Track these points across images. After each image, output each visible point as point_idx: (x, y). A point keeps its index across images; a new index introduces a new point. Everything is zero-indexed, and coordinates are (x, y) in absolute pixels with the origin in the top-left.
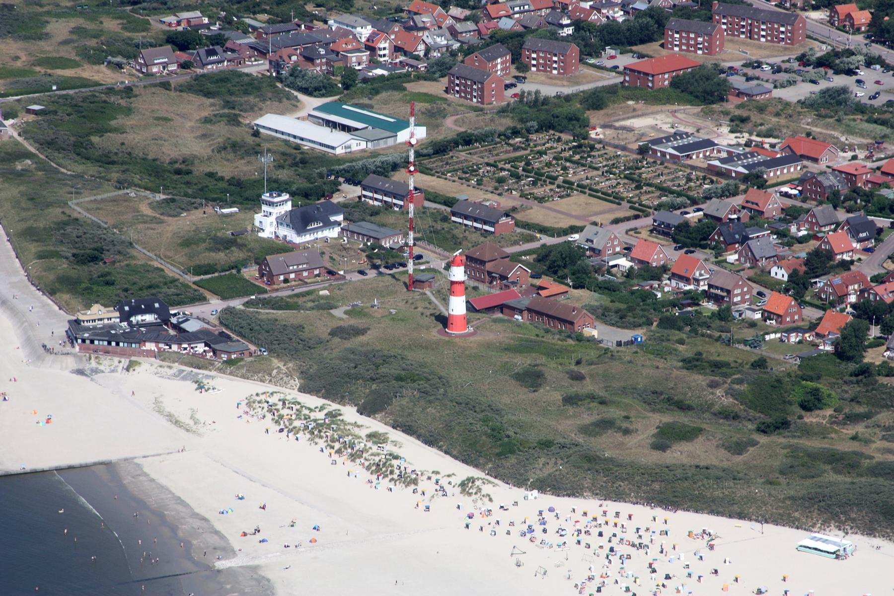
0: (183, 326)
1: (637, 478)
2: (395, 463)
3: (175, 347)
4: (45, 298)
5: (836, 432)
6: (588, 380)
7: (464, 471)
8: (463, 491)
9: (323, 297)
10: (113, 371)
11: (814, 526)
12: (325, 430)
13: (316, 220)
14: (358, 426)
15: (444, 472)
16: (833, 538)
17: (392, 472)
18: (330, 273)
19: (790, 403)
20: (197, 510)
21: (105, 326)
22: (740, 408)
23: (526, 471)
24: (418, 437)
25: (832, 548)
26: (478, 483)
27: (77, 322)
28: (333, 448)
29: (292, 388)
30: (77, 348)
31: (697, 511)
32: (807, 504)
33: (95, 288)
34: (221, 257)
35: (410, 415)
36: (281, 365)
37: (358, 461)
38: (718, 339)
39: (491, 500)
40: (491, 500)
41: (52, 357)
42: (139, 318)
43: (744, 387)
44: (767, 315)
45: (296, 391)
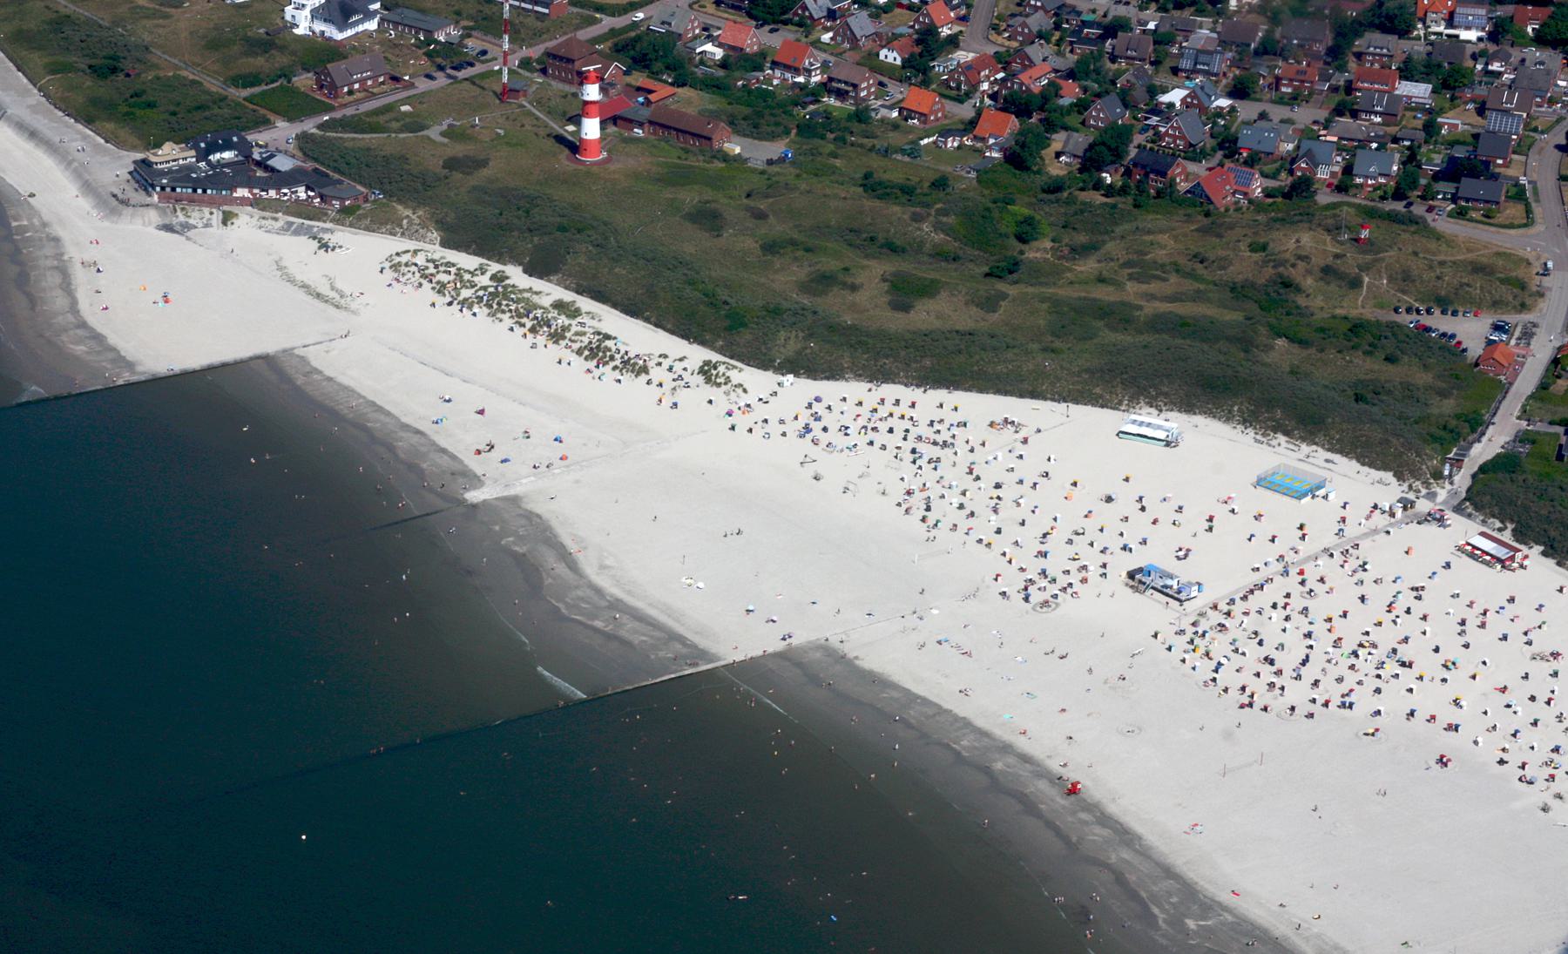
0: (270, 162)
1: (903, 353)
2: (609, 343)
3: (272, 193)
4: (80, 127)
5: (1070, 270)
6: (772, 219)
7: (698, 354)
8: (708, 380)
9: (406, 114)
10: (207, 226)
11: (1120, 403)
12: (498, 299)
13: (356, 12)
14: (537, 293)
15: (674, 355)
16: (1148, 419)
17: (612, 358)
18: (395, 79)
19: (1007, 236)
20: (404, 420)
21: (182, 168)
22: (953, 246)
23: (769, 349)
24: (615, 306)
25: (1162, 435)
26: (722, 369)
27: (145, 163)
28: (523, 325)
29: (432, 242)
30: (156, 197)
31: (981, 391)
32: (1107, 377)
33: (138, 112)
34: (259, 62)
35: (594, 277)
36: (409, 212)
37: (563, 343)
38: (872, 149)
39: (745, 391)
40: (745, 391)
41: (130, 210)
42: (218, 156)
43: (951, 220)
44: (906, 114)
45: (437, 247)
